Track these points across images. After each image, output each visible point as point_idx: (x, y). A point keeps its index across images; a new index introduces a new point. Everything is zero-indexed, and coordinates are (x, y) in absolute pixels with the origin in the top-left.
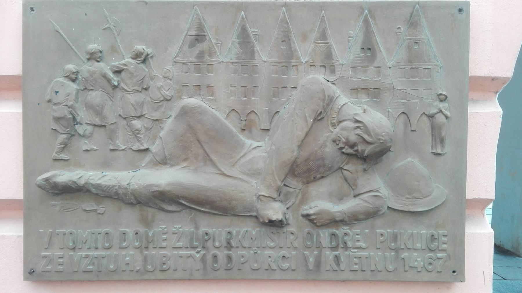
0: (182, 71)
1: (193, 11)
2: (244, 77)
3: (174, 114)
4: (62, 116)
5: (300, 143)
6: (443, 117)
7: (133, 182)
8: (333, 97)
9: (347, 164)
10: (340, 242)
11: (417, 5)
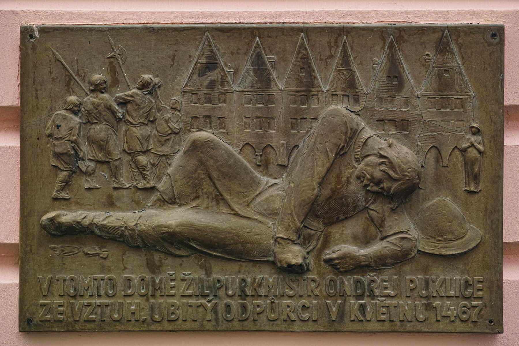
0: (191, 102)
1: (204, 37)
2: (259, 107)
3: (183, 148)
4: (65, 151)
5: (321, 180)
6: (475, 151)
7: (140, 222)
8: (356, 130)
9: (373, 203)
10: (366, 290)
11: (447, 31)
